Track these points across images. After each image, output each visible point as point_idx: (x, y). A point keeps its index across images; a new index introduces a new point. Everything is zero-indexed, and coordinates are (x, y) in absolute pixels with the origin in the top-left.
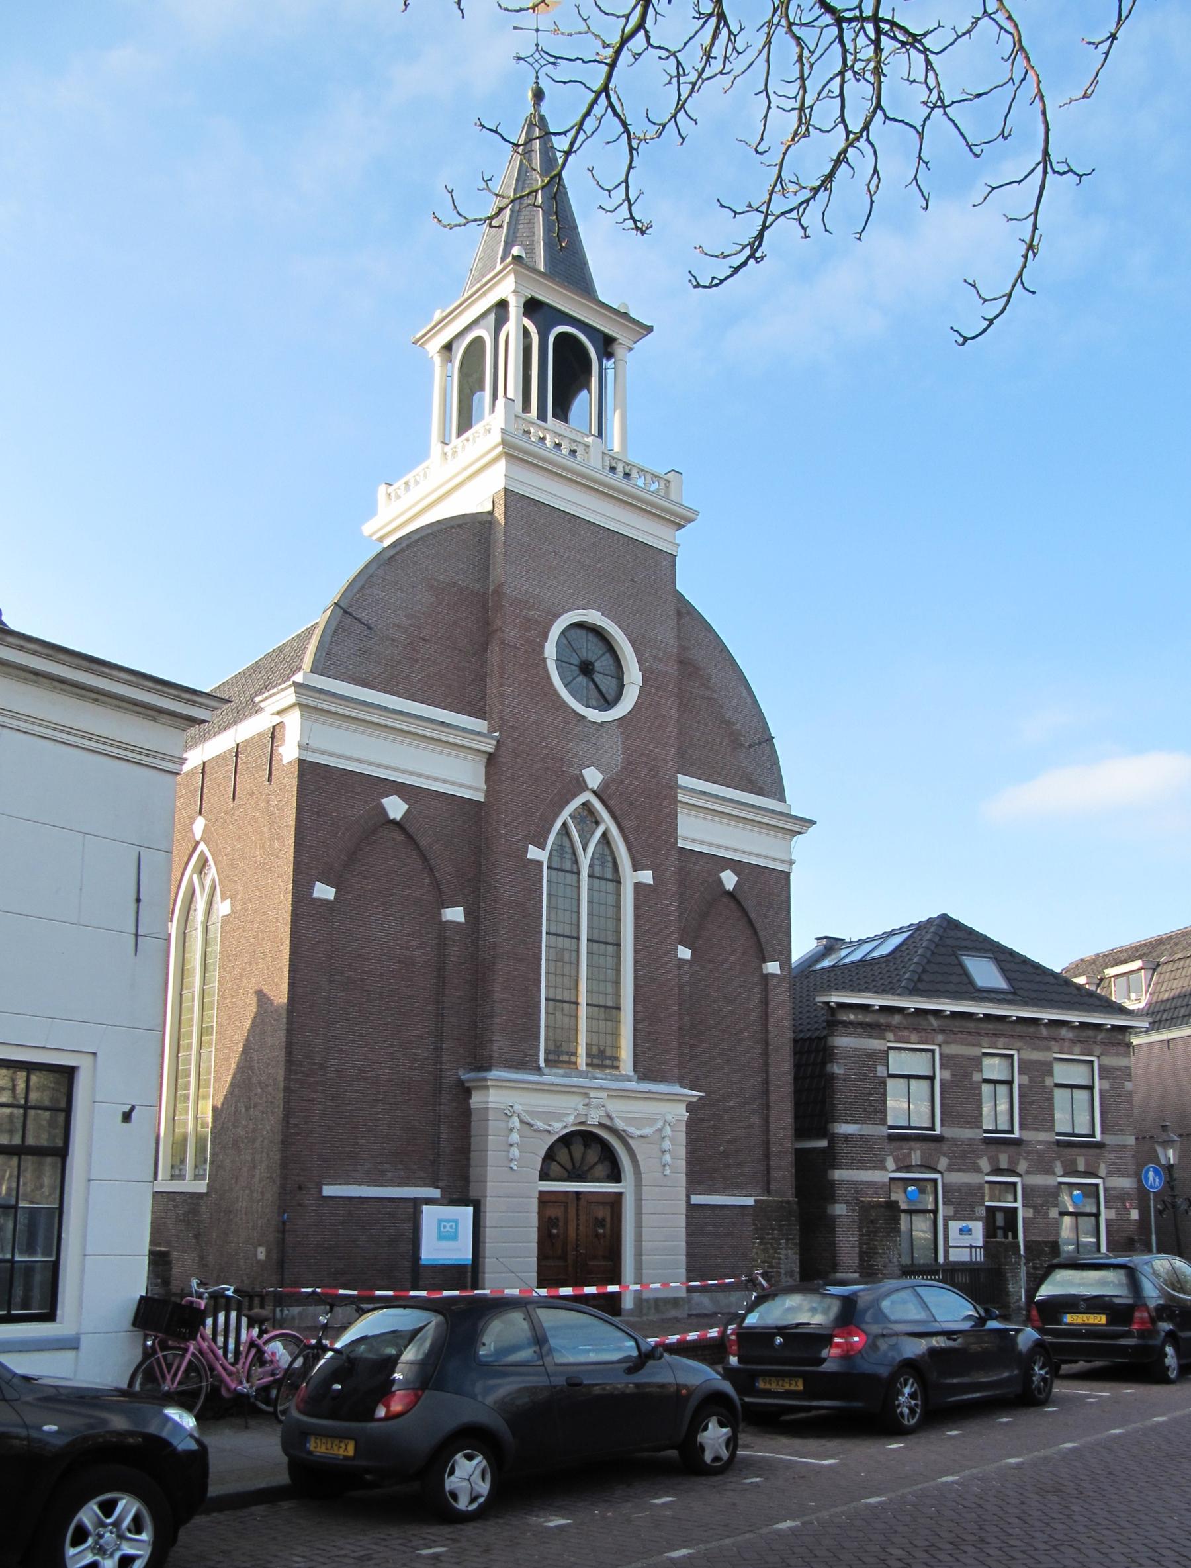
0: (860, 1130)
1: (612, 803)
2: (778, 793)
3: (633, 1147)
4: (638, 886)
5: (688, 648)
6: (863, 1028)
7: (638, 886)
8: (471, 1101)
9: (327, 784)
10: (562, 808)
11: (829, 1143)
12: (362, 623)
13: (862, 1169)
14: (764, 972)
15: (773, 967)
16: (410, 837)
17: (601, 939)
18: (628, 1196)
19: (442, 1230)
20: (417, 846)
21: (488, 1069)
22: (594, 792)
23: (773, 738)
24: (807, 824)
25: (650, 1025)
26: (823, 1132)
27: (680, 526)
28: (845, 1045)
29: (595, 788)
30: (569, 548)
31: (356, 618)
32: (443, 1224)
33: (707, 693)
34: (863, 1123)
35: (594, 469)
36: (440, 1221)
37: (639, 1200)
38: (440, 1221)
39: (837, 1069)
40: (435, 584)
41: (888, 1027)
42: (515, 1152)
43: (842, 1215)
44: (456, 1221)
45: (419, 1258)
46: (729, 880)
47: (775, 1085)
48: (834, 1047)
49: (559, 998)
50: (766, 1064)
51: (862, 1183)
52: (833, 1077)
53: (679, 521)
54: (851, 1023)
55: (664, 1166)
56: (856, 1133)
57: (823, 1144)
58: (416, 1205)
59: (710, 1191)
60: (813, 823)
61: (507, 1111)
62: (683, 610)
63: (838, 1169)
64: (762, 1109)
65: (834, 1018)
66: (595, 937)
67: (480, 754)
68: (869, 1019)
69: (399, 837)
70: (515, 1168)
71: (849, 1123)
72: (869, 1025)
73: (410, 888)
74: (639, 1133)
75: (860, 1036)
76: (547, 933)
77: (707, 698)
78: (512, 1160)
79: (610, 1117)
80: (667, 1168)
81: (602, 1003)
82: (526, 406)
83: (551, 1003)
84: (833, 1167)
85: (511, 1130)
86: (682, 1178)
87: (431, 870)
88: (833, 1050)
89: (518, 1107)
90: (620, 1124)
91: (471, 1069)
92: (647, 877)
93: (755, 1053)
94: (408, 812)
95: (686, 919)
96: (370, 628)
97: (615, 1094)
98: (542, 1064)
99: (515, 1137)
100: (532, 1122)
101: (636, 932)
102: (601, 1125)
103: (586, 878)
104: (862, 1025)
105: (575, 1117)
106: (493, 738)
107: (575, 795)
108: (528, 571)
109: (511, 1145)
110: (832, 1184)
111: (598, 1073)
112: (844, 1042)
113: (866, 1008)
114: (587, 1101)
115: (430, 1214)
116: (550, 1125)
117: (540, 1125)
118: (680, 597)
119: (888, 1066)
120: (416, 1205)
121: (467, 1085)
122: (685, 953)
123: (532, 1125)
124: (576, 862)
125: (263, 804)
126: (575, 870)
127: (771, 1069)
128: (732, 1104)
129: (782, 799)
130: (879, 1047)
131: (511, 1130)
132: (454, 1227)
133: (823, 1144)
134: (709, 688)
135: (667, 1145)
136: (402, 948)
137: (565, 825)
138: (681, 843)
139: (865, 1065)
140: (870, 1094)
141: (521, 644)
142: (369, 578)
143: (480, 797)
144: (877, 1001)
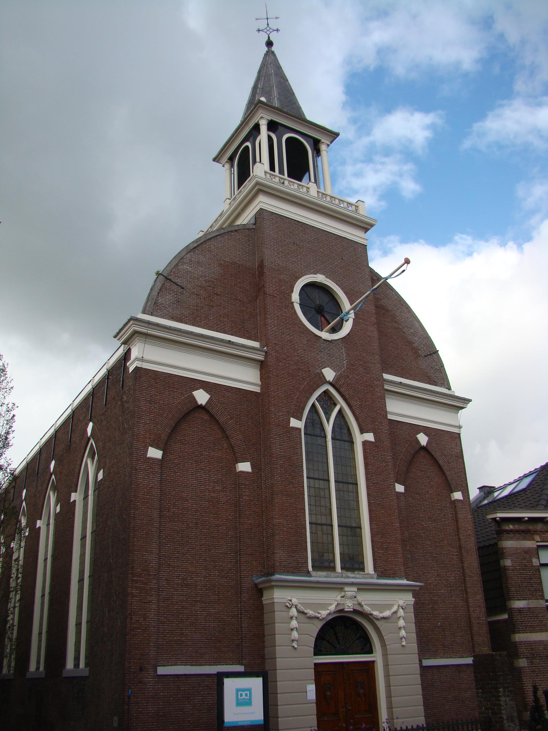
0: (528, 604)
1: (342, 390)
2: (444, 381)
3: (379, 626)
4: (365, 443)
5: (381, 299)
6: (519, 534)
7: (365, 443)
8: (263, 599)
9: (156, 383)
10: (311, 394)
11: (509, 616)
12: (178, 285)
13: (534, 632)
14: (453, 499)
15: (458, 495)
16: (212, 416)
17: (344, 481)
18: (378, 662)
19: (239, 697)
20: (217, 422)
21: (273, 574)
22: (331, 384)
23: (438, 351)
24: (466, 402)
25: (382, 537)
26: (504, 608)
27: (366, 230)
28: (510, 546)
29: (331, 380)
30: (302, 241)
31: (174, 282)
32: (239, 693)
33: (396, 325)
34: (529, 599)
35: (313, 197)
36: (238, 690)
37: (386, 666)
38: (238, 690)
39: (508, 562)
40: (223, 263)
41: (536, 532)
42: (295, 634)
43: (525, 667)
44: (250, 690)
45: (223, 721)
46: (423, 439)
47: (469, 576)
48: (503, 548)
49: (319, 522)
50: (462, 562)
51: (535, 642)
52: (505, 568)
53: (365, 227)
54: (511, 531)
55: (401, 638)
56: (526, 606)
57: (505, 616)
58: (220, 677)
59: (435, 656)
60: (469, 401)
61: (288, 604)
62: (375, 278)
63: (518, 633)
64: (463, 594)
65: (500, 529)
66: (340, 480)
67: (256, 362)
68: (522, 527)
69: (206, 417)
70: (296, 646)
71: (520, 600)
72: (523, 531)
73: (213, 451)
74: (381, 615)
75: (518, 539)
76: (307, 478)
77: (395, 328)
78: (293, 640)
79: (360, 604)
80: (404, 640)
81: (348, 524)
82: (272, 168)
83: (314, 526)
84: (514, 632)
85: (292, 618)
86: (414, 646)
87: (227, 437)
88: (503, 550)
89: (295, 601)
90: (367, 609)
91: (261, 575)
92: (370, 437)
93: (453, 555)
94: (210, 399)
95: (399, 466)
96: (183, 288)
97: (363, 588)
98: (310, 568)
99: (294, 623)
100: (305, 611)
101: (367, 474)
102: (355, 611)
103: (331, 440)
104: (518, 531)
105: (336, 606)
106: (262, 351)
107: (318, 386)
108: (278, 253)
109: (292, 630)
110: (515, 645)
111: (350, 574)
112: (509, 544)
113: (519, 520)
114: (343, 594)
115: (230, 684)
116: (319, 613)
117: (311, 612)
118: (372, 271)
119: (539, 558)
120: (220, 677)
121: (260, 586)
122: (400, 488)
123: (306, 614)
124: (323, 429)
125: (119, 403)
126: (323, 435)
127: (465, 565)
128: (443, 591)
129: (449, 389)
130: (531, 546)
131: (292, 618)
132: (248, 695)
133: (505, 616)
134: (395, 322)
135: (401, 623)
136: (210, 491)
137: (313, 405)
138: (390, 417)
139: (524, 559)
140: (531, 579)
141: (278, 295)
142: (181, 259)
143: (257, 389)
144: (526, 515)
